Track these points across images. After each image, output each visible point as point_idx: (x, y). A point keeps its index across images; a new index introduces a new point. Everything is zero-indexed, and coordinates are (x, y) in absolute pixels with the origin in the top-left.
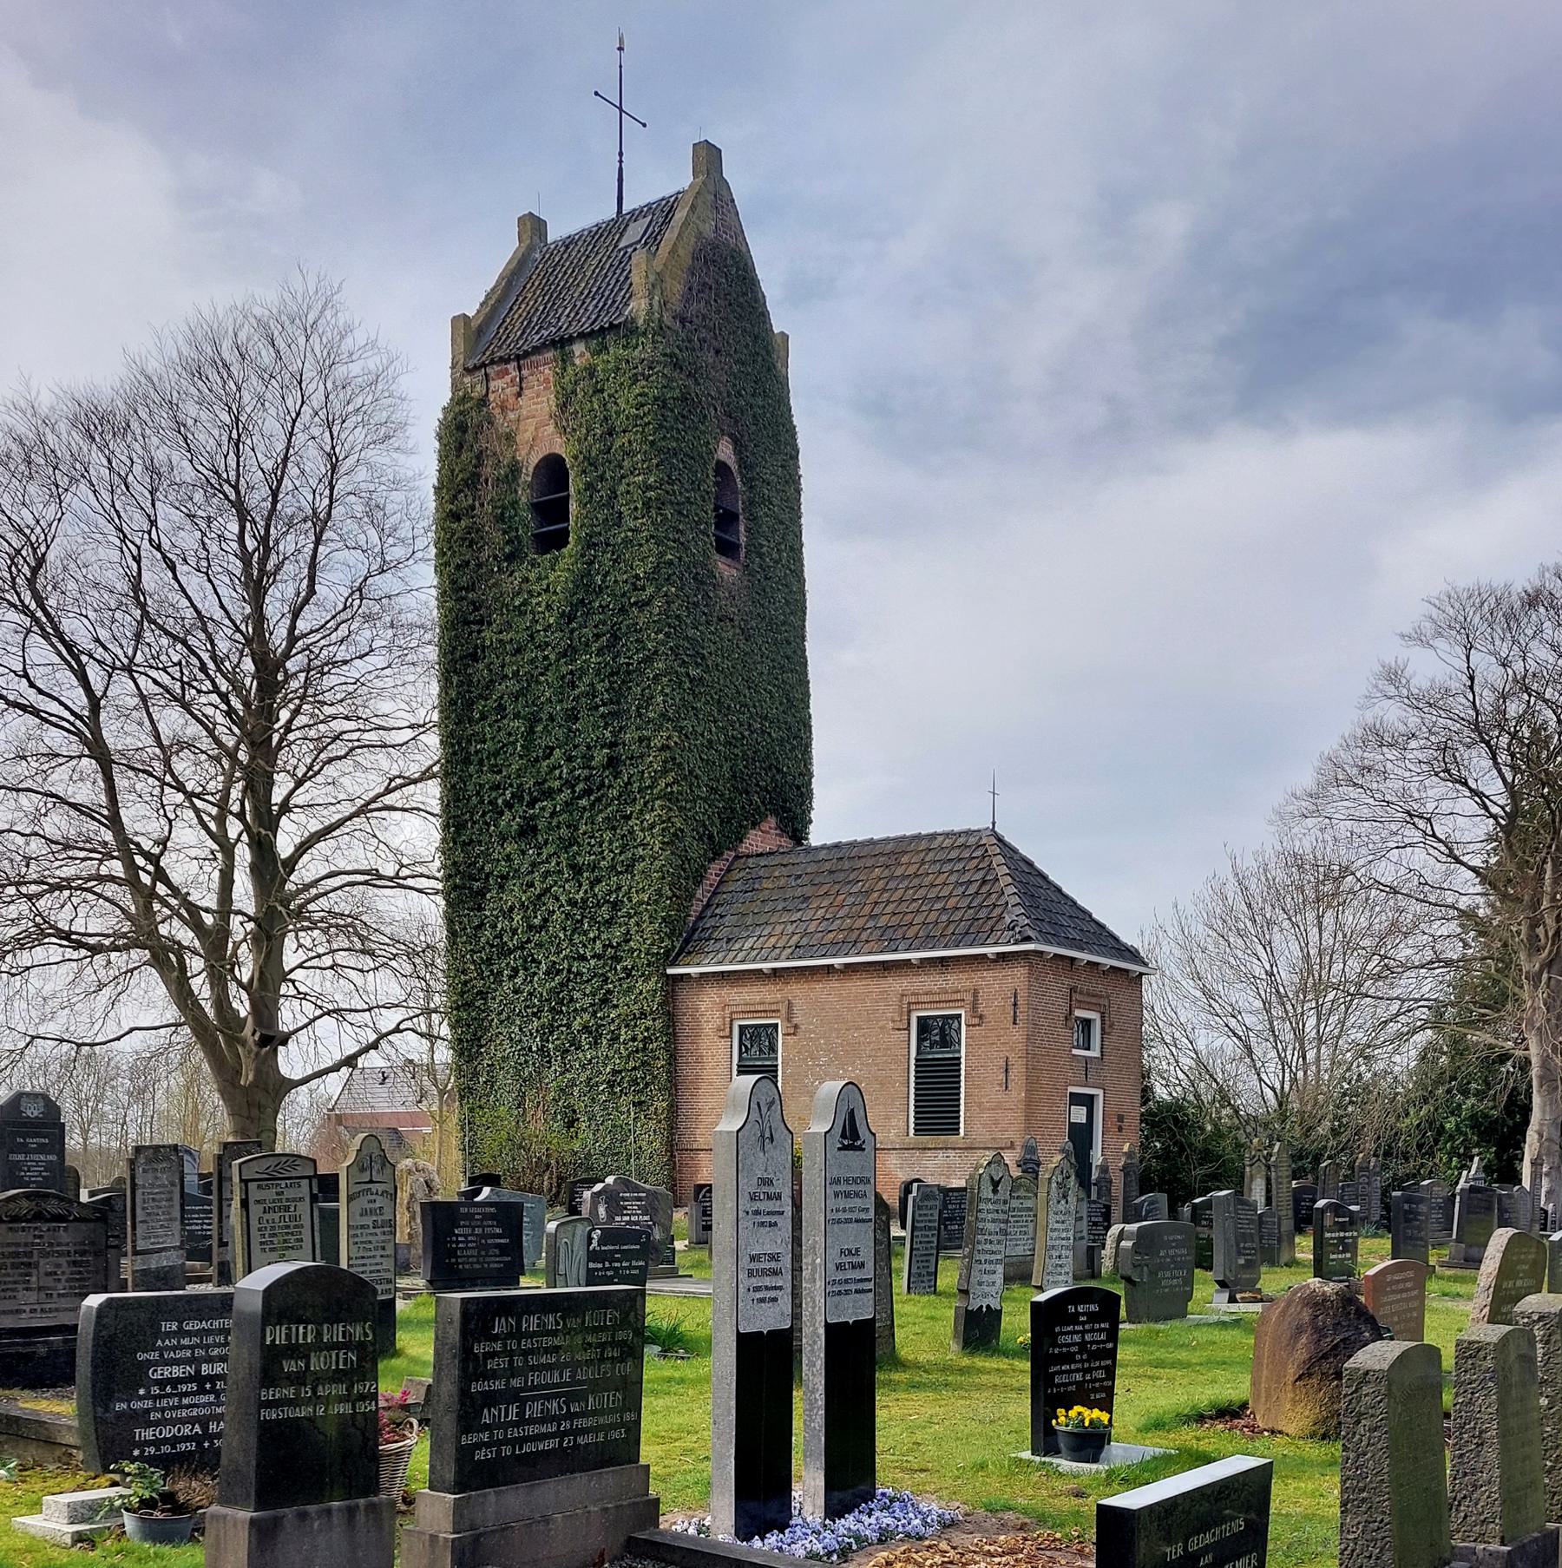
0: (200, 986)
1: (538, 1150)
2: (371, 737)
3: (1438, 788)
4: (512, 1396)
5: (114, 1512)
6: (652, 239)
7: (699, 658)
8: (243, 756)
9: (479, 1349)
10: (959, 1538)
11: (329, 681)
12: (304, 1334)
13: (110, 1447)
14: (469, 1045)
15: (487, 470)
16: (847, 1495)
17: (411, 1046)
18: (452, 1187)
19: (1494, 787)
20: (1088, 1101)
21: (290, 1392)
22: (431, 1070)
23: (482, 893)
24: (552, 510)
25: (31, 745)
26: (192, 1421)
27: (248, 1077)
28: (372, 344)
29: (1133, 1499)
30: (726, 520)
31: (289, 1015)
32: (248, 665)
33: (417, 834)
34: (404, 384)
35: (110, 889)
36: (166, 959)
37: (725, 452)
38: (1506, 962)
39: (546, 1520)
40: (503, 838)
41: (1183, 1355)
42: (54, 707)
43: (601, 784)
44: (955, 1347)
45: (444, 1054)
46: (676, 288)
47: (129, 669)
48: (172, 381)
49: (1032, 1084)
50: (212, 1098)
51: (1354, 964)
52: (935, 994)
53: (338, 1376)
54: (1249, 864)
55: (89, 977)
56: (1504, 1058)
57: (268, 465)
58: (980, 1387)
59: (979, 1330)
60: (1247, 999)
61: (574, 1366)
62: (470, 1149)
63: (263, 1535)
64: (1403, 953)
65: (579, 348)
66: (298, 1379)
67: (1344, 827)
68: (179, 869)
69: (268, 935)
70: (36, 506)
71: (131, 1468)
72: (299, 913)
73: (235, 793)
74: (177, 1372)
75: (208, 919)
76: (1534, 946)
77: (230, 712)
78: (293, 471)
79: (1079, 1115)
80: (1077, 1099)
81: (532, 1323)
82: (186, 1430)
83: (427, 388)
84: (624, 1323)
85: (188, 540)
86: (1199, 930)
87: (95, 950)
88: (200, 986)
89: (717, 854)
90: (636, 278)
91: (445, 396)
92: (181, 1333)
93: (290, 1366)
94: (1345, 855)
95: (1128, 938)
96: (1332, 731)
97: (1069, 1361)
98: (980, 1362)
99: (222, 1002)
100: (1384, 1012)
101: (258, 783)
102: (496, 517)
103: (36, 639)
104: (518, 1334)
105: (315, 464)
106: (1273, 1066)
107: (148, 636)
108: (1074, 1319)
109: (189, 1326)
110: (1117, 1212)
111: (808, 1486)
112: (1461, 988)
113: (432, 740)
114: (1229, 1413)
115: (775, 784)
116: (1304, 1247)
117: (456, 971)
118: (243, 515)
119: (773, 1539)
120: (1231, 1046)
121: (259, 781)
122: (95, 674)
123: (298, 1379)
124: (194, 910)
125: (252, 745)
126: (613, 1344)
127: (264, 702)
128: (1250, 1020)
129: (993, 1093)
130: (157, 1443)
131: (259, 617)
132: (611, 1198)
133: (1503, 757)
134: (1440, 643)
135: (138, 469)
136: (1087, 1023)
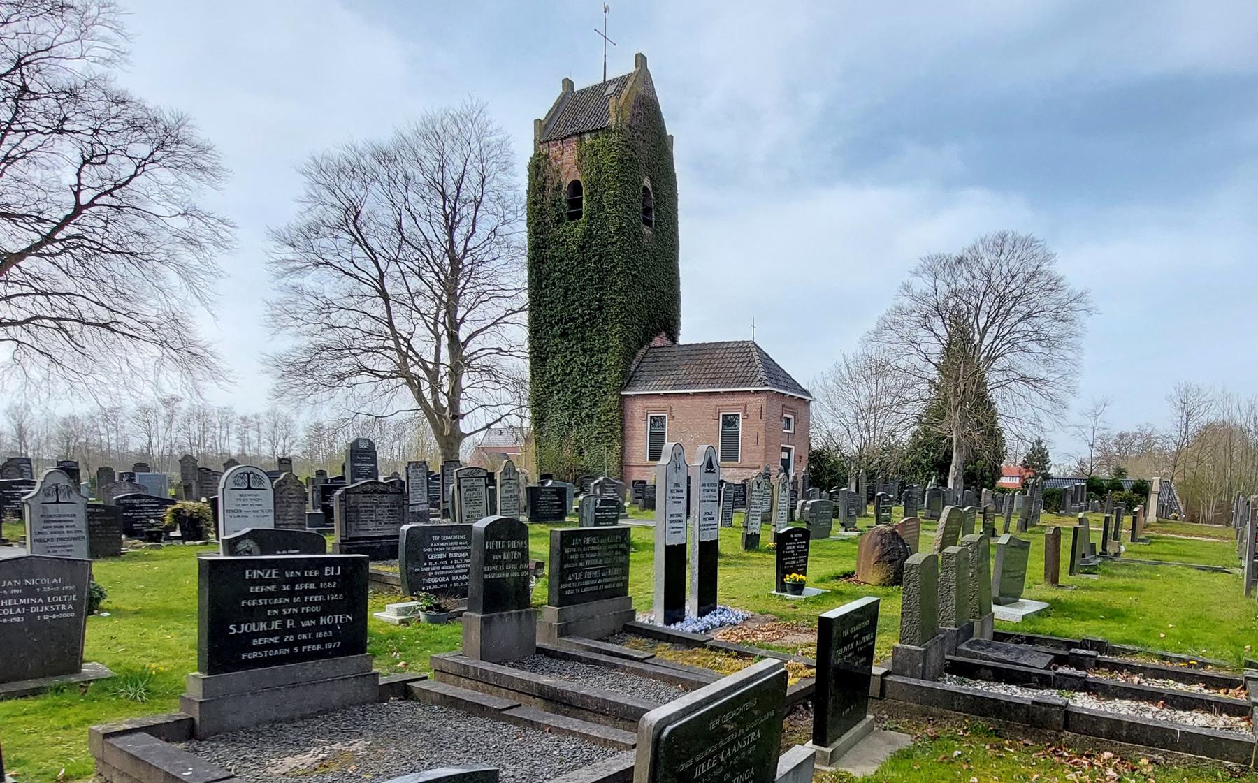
0: (427, 394)
1: (567, 464)
2: (500, 293)
3: (923, 332)
4: (579, 569)
5: (415, 611)
6: (618, 92)
7: (635, 267)
8: (445, 299)
9: (567, 551)
10: (749, 624)
11: (481, 269)
12: (501, 545)
13: (413, 586)
14: (539, 421)
15: (548, 185)
16: (705, 608)
17: (514, 420)
18: (535, 481)
19: (943, 333)
20: (789, 450)
21: (495, 568)
22: (521, 429)
23: (545, 359)
24: (575, 203)
25: (355, 291)
26: (445, 576)
27: (447, 432)
28: (499, 129)
29: (833, 614)
30: (647, 211)
31: (464, 407)
32: (447, 261)
33: (518, 333)
34: (513, 147)
35: (388, 353)
36: (412, 381)
37: (647, 182)
38: (945, 401)
39: (593, 618)
40: (554, 337)
41: (829, 552)
42: (364, 275)
43: (596, 316)
44: (742, 548)
45: (527, 423)
46: (627, 114)
47: (395, 260)
48: (413, 139)
49: (767, 443)
50: (432, 439)
51: (889, 399)
52: (730, 406)
53: (513, 562)
54: (850, 358)
55: (381, 389)
56: (944, 438)
57: (456, 178)
58: (752, 565)
59: (751, 542)
60: (849, 411)
61: (604, 558)
62: (540, 463)
63: (486, 622)
64: (907, 395)
65: (587, 136)
66: (498, 563)
67: (887, 346)
68: (417, 345)
69: (455, 374)
70: (356, 192)
71: (422, 594)
72: (468, 365)
73: (442, 314)
74: (439, 556)
75: (430, 366)
76: (956, 395)
77: (440, 280)
78: (466, 180)
79: (785, 455)
80: (784, 449)
81: (587, 541)
82: (443, 579)
83: (524, 149)
84: (622, 541)
85: (422, 207)
86: (830, 383)
87: (383, 378)
88: (427, 394)
89: (642, 346)
90: (611, 109)
91: (531, 153)
92: (440, 541)
93: (495, 557)
94: (887, 356)
95: (805, 387)
96: (883, 308)
97: (790, 554)
98: (752, 554)
99: (436, 401)
100: (899, 419)
101: (451, 311)
102: (553, 205)
103: (356, 246)
104: (581, 545)
105: (476, 178)
106: (857, 437)
107: (405, 247)
108: (792, 540)
109: (444, 538)
110: (799, 495)
111: (691, 604)
112: (928, 410)
113: (525, 295)
114: (848, 575)
115: (664, 317)
116: (871, 509)
117: (534, 390)
118: (445, 197)
119: (679, 625)
120: (842, 429)
121: (452, 310)
122: (381, 261)
123: (498, 563)
124: (423, 361)
125: (449, 295)
126: (619, 549)
127: (454, 274)
128: (849, 419)
129: (752, 446)
130: (432, 584)
131: (452, 242)
132: (601, 485)
133: (947, 322)
134: (924, 275)
135: (400, 176)
136: (789, 419)
